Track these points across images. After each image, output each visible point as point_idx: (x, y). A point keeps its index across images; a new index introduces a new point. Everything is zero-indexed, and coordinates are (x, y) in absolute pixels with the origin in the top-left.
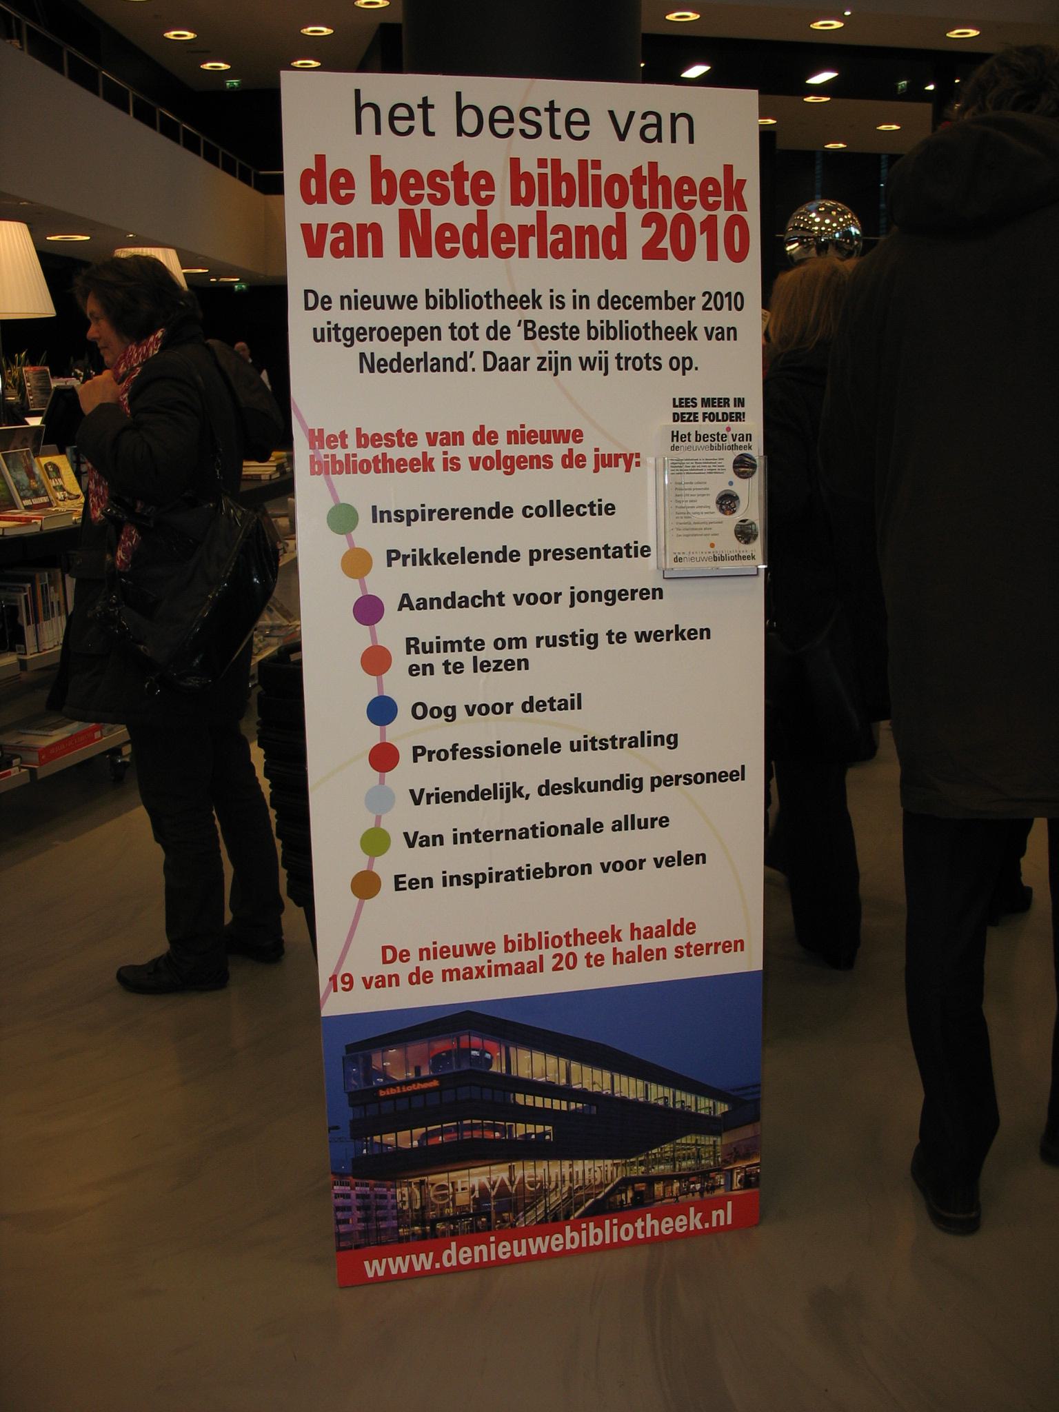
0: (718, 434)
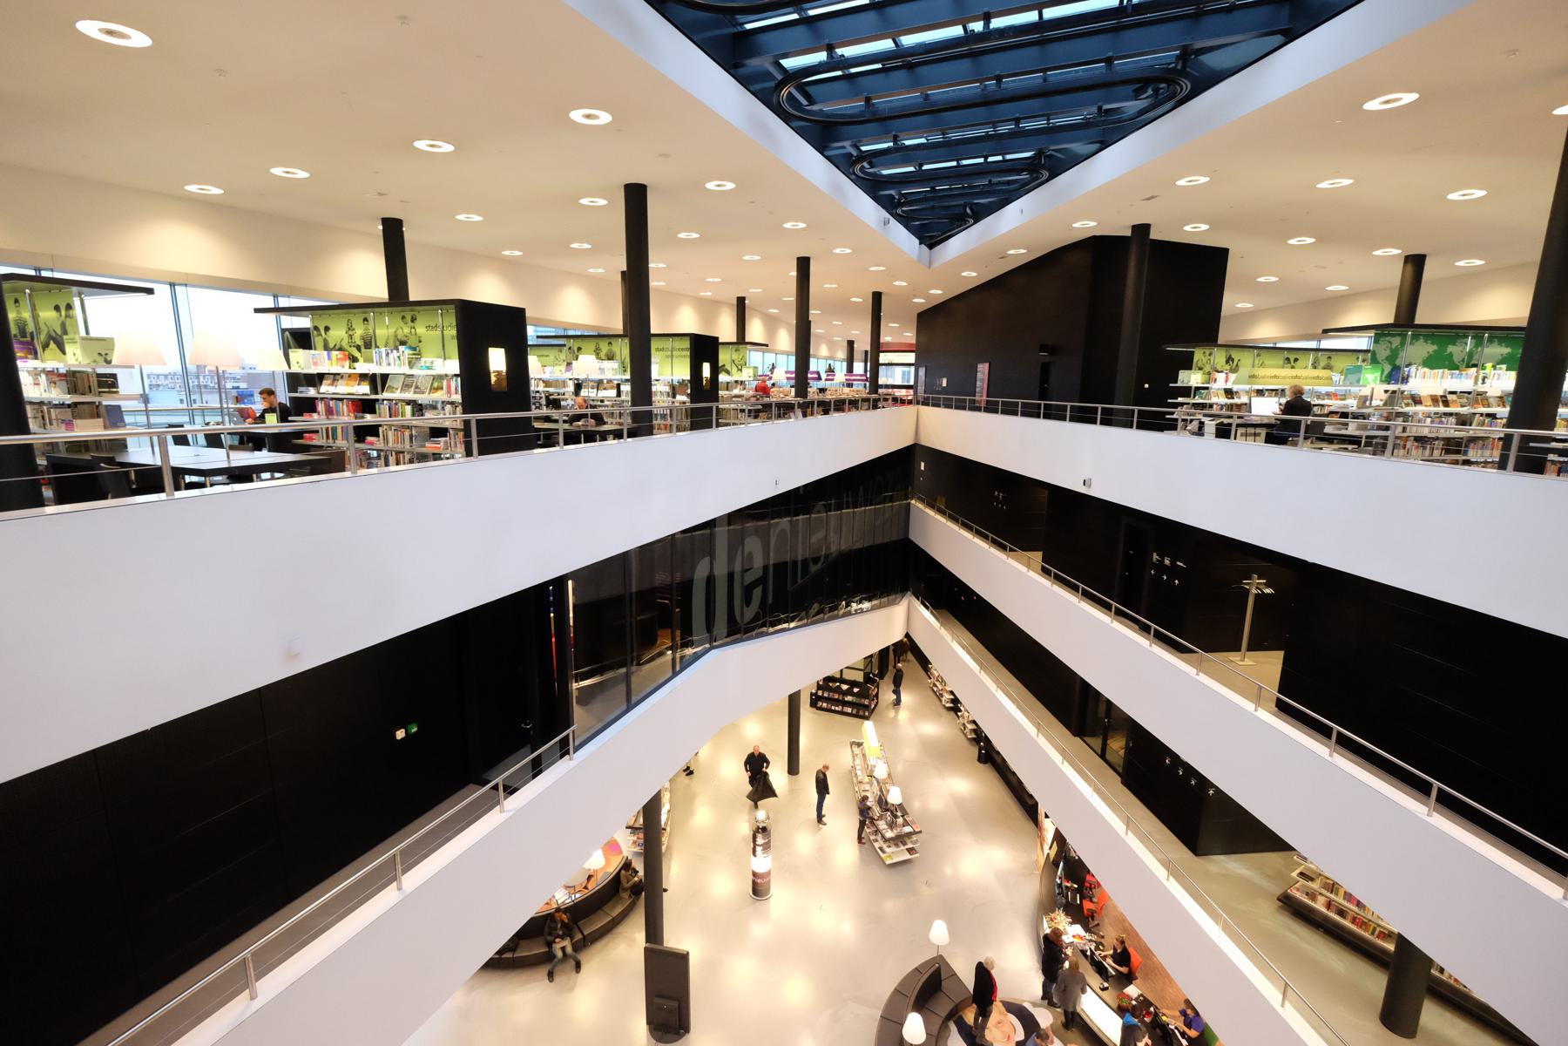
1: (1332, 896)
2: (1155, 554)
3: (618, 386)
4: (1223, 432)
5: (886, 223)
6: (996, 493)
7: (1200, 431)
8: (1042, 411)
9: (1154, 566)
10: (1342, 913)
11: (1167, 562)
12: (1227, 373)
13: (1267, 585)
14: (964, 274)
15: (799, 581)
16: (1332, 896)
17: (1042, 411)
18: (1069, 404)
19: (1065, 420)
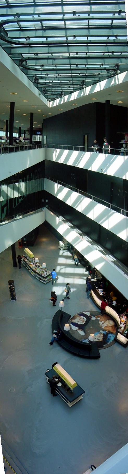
5: (40, 95)
15: (16, 205)
18: (80, 147)
19: (103, 153)
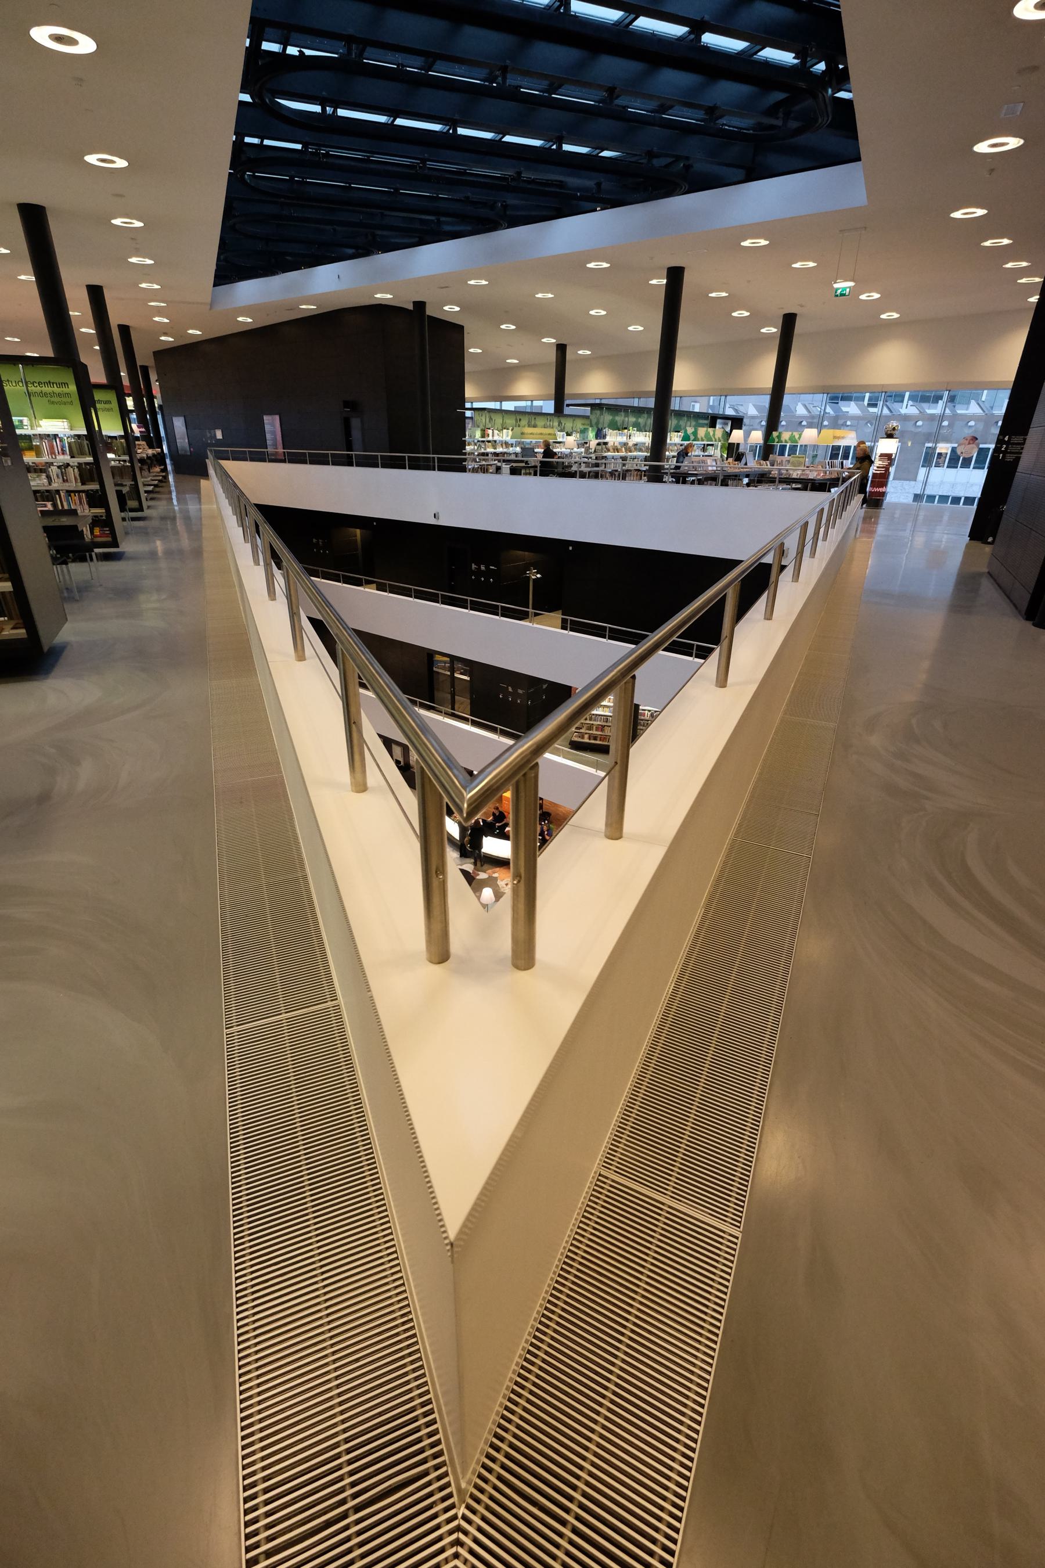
0: (50, 382)
1: (591, 732)
2: (473, 564)
3: (580, 464)
4: (514, 472)
6: (314, 540)
7: (498, 470)
8: (436, 464)
9: (473, 573)
10: (595, 738)
11: (483, 568)
12: (493, 430)
13: (537, 573)
14: (240, 319)
16: (591, 732)
17: (436, 464)
